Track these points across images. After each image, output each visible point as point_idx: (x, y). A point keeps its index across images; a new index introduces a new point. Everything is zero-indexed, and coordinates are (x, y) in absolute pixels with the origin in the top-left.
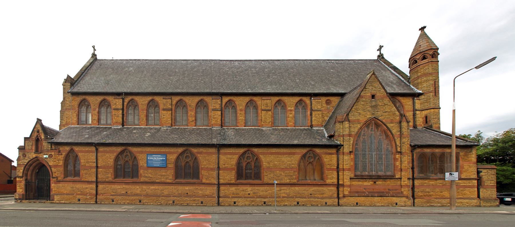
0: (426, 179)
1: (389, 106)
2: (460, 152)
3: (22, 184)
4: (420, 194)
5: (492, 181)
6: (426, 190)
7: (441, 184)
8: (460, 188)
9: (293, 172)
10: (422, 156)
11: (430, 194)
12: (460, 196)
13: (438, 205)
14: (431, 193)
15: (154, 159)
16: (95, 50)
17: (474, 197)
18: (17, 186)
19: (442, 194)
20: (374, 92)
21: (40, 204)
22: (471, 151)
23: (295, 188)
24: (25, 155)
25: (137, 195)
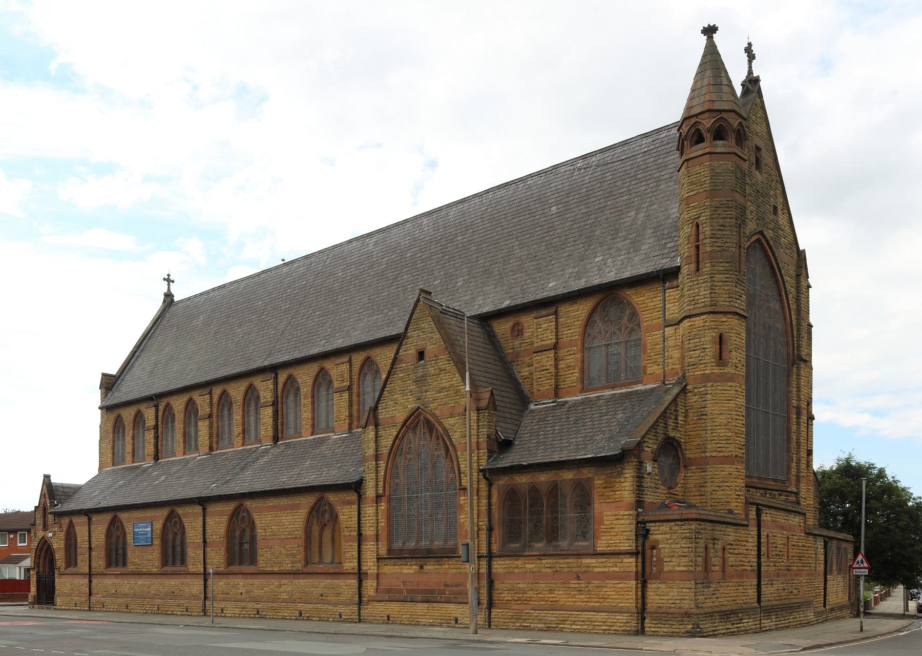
1: (447, 374)
2: (596, 479)
4: (506, 596)
5: (684, 559)
7: (549, 570)
8: (592, 580)
9: (296, 546)
10: (511, 496)
12: (594, 604)
13: (539, 625)
14: (528, 592)
15: (140, 531)
16: (751, 57)
19: (552, 596)
20: (421, 344)
21: (55, 611)
22: (620, 474)
23: (300, 581)
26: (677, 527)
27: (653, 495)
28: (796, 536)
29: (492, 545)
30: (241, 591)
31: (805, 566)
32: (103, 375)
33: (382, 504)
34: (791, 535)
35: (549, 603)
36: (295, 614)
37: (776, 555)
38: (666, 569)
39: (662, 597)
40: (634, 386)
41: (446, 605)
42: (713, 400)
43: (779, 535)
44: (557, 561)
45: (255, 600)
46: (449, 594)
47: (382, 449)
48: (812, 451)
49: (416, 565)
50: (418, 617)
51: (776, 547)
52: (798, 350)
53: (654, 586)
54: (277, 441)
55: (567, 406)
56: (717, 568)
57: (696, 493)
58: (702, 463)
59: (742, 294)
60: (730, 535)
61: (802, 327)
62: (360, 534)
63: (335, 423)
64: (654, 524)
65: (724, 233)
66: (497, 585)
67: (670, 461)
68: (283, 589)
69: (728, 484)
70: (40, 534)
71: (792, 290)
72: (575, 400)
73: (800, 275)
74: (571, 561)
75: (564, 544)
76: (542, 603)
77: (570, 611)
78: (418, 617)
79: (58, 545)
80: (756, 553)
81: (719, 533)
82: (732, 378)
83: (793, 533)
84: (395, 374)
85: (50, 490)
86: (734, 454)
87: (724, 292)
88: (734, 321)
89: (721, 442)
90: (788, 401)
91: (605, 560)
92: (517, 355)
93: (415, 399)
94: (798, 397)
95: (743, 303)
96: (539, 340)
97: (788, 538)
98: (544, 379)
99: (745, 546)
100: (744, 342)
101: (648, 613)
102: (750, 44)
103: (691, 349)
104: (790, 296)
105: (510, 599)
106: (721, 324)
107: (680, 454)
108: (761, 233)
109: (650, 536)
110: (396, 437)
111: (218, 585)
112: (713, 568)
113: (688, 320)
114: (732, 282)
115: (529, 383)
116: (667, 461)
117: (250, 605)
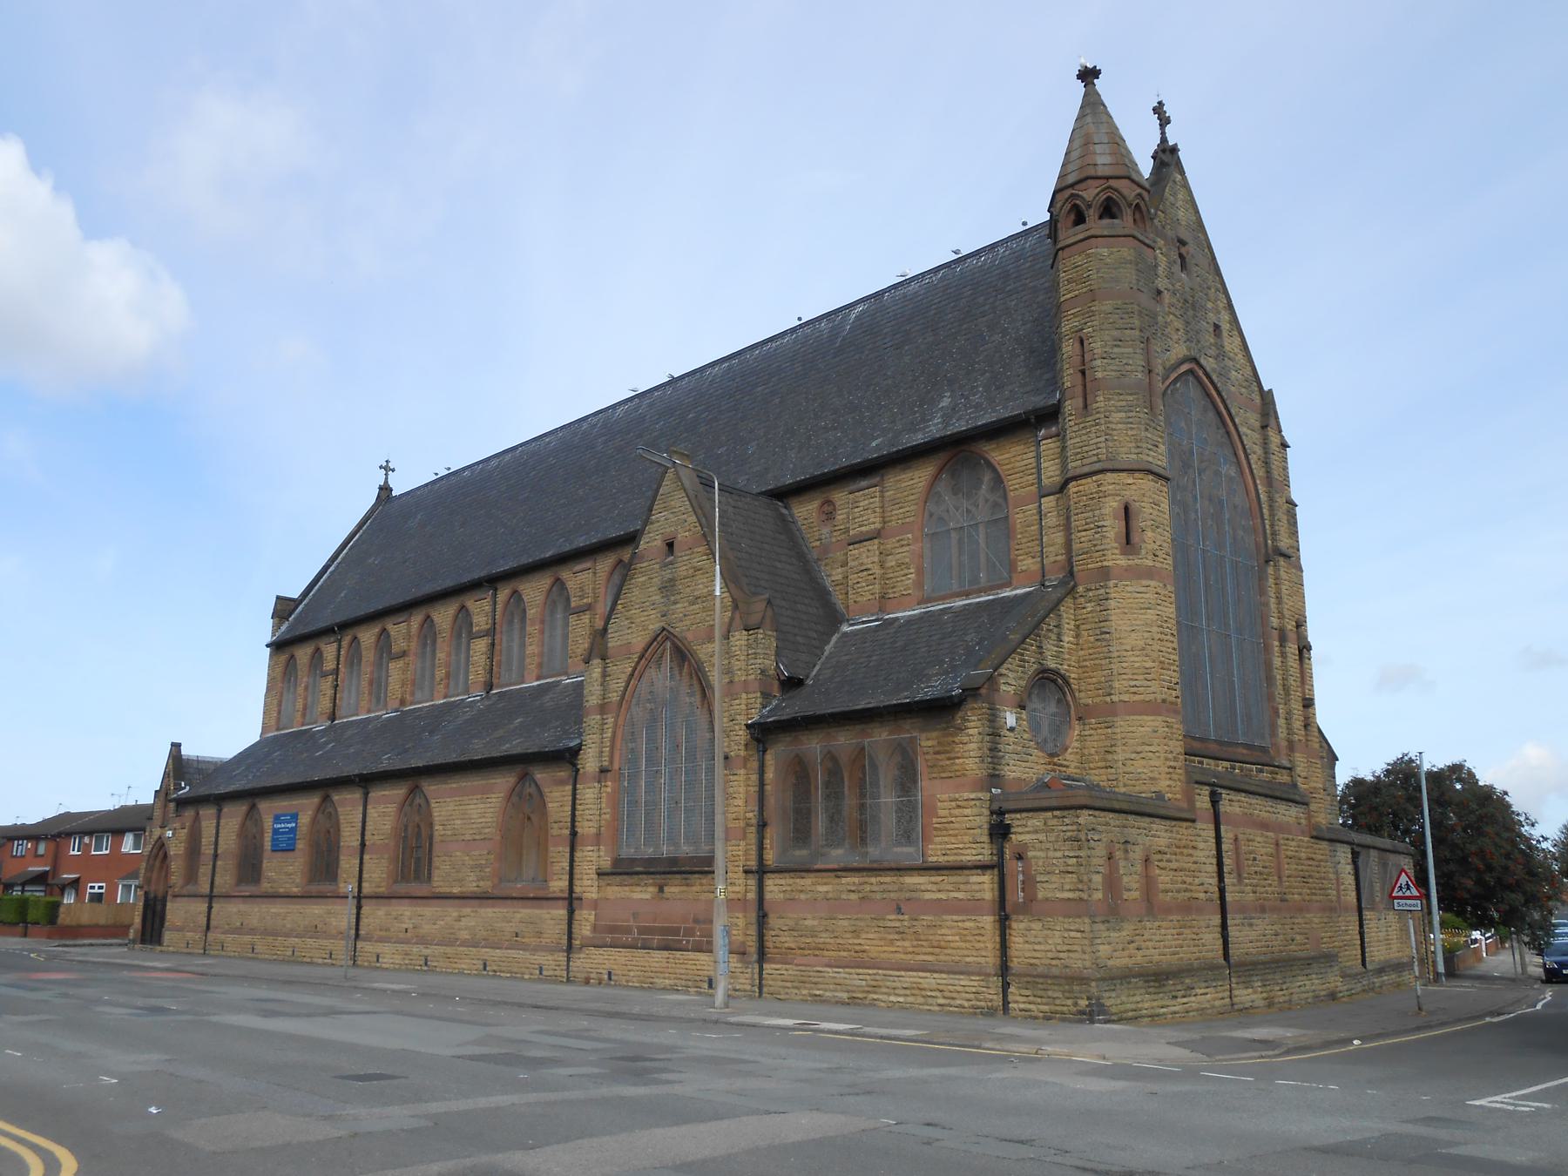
4: (788, 940)
6: (806, 923)
7: (853, 896)
10: (800, 772)
11: (817, 940)
16: (1164, 121)
17: (979, 959)
19: (856, 941)
26: (1056, 820)
27: (1020, 766)
28: (1293, 840)
29: (765, 852)
30: (405, 926)
31: (1315, 894)
32: (278, 598)
33: (609, 783)
34: (1283, 838)
35: (852, 953)
36: (475, 967)
37: (1256, 872)
38: (1040, 895)
39: (1037, 947)
40: (999, 591)
41: (691, 955)
42: (1119, 608)
43: (1259, 839)
44: (866, 879)
45: (424, 941)
46: (700, 936)
47: (610, 695)
48: (1312, 700)
49: (653, 885)
50: (652, 975)
51: (1255, 859)
52: (1274, 540)
53: (1022, 926)
54: (491, 689)
55: (896, 624)
56: (1135, 895)
57: (1100, 764)
58: (1108, 712)
59: (1158, 442)
60: (1160, 835)
61: (1277, 504)
62: (574, 834)
63: (570, 661)
64: (1018, 816)
65: (1123, 350)
66: (773, 921)
67: (1052, 708)
68: (464, 922)
69: (1151, 748)
70: (157, 832)
71: (1256, 452)
72: (910, 616)
73: (1267, 426)
74: (888, 879)
75: (874, 852)
76: (843, 954)
77: (886, 969)
78: (652, 975)
79: (176, 849)
80: (1215, 868)
81: (1134, 831)
82: (1149, 573)
83: (1286, 836)
84: (632, 578)
85: (178, 765)
86: (1159, 697)
87: (1128, 439)
88: (1147, 483)
89: (1136, 677)
90: (1264, 618)
91: (941, 878)
92: (825, 549)
93: (659, 615)
94: (1279, 612)
95: (1160, 457)
96: (857, 525)
97: (1277, 844)
98: (864, 584)
99: (1191, 855)
100: (1167, 517)
101: (1013, 975)
102: (1160, 103)
103: (1080, 528)
104: (1253, 458)
105: (793, 945)
106: (1124, 488)
107: (1069, 698)
108: (1195, 360)
109: (1013, 836)
110: (632, 675)
112: (1126, 895)
113: (1074, 483)
114: (1140, 423)
115: (843, 591)
116: (1046, 709)
117: (415, 949)
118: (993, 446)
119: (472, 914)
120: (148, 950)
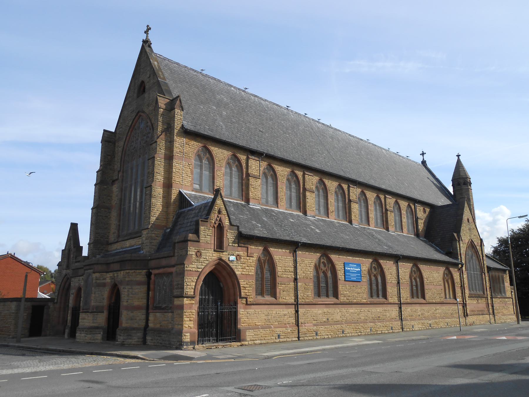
0: (34, 268)
3: (194, 311)
18: (184, 316)
24: (198, 254)
25: (337, 323)
30: (418, 314)
32: (105, 131)
45: (426, 318)
111: (407, 310)
117: (426, 322)
118: (160, 73)
119: (439, 309)
120: (220, 347)
